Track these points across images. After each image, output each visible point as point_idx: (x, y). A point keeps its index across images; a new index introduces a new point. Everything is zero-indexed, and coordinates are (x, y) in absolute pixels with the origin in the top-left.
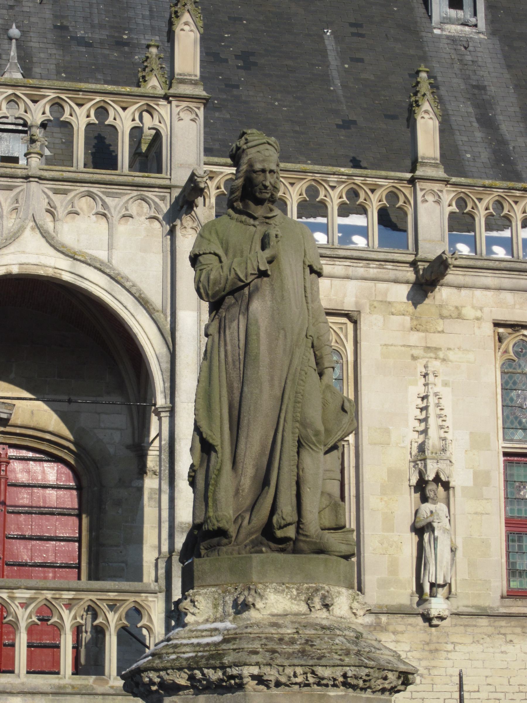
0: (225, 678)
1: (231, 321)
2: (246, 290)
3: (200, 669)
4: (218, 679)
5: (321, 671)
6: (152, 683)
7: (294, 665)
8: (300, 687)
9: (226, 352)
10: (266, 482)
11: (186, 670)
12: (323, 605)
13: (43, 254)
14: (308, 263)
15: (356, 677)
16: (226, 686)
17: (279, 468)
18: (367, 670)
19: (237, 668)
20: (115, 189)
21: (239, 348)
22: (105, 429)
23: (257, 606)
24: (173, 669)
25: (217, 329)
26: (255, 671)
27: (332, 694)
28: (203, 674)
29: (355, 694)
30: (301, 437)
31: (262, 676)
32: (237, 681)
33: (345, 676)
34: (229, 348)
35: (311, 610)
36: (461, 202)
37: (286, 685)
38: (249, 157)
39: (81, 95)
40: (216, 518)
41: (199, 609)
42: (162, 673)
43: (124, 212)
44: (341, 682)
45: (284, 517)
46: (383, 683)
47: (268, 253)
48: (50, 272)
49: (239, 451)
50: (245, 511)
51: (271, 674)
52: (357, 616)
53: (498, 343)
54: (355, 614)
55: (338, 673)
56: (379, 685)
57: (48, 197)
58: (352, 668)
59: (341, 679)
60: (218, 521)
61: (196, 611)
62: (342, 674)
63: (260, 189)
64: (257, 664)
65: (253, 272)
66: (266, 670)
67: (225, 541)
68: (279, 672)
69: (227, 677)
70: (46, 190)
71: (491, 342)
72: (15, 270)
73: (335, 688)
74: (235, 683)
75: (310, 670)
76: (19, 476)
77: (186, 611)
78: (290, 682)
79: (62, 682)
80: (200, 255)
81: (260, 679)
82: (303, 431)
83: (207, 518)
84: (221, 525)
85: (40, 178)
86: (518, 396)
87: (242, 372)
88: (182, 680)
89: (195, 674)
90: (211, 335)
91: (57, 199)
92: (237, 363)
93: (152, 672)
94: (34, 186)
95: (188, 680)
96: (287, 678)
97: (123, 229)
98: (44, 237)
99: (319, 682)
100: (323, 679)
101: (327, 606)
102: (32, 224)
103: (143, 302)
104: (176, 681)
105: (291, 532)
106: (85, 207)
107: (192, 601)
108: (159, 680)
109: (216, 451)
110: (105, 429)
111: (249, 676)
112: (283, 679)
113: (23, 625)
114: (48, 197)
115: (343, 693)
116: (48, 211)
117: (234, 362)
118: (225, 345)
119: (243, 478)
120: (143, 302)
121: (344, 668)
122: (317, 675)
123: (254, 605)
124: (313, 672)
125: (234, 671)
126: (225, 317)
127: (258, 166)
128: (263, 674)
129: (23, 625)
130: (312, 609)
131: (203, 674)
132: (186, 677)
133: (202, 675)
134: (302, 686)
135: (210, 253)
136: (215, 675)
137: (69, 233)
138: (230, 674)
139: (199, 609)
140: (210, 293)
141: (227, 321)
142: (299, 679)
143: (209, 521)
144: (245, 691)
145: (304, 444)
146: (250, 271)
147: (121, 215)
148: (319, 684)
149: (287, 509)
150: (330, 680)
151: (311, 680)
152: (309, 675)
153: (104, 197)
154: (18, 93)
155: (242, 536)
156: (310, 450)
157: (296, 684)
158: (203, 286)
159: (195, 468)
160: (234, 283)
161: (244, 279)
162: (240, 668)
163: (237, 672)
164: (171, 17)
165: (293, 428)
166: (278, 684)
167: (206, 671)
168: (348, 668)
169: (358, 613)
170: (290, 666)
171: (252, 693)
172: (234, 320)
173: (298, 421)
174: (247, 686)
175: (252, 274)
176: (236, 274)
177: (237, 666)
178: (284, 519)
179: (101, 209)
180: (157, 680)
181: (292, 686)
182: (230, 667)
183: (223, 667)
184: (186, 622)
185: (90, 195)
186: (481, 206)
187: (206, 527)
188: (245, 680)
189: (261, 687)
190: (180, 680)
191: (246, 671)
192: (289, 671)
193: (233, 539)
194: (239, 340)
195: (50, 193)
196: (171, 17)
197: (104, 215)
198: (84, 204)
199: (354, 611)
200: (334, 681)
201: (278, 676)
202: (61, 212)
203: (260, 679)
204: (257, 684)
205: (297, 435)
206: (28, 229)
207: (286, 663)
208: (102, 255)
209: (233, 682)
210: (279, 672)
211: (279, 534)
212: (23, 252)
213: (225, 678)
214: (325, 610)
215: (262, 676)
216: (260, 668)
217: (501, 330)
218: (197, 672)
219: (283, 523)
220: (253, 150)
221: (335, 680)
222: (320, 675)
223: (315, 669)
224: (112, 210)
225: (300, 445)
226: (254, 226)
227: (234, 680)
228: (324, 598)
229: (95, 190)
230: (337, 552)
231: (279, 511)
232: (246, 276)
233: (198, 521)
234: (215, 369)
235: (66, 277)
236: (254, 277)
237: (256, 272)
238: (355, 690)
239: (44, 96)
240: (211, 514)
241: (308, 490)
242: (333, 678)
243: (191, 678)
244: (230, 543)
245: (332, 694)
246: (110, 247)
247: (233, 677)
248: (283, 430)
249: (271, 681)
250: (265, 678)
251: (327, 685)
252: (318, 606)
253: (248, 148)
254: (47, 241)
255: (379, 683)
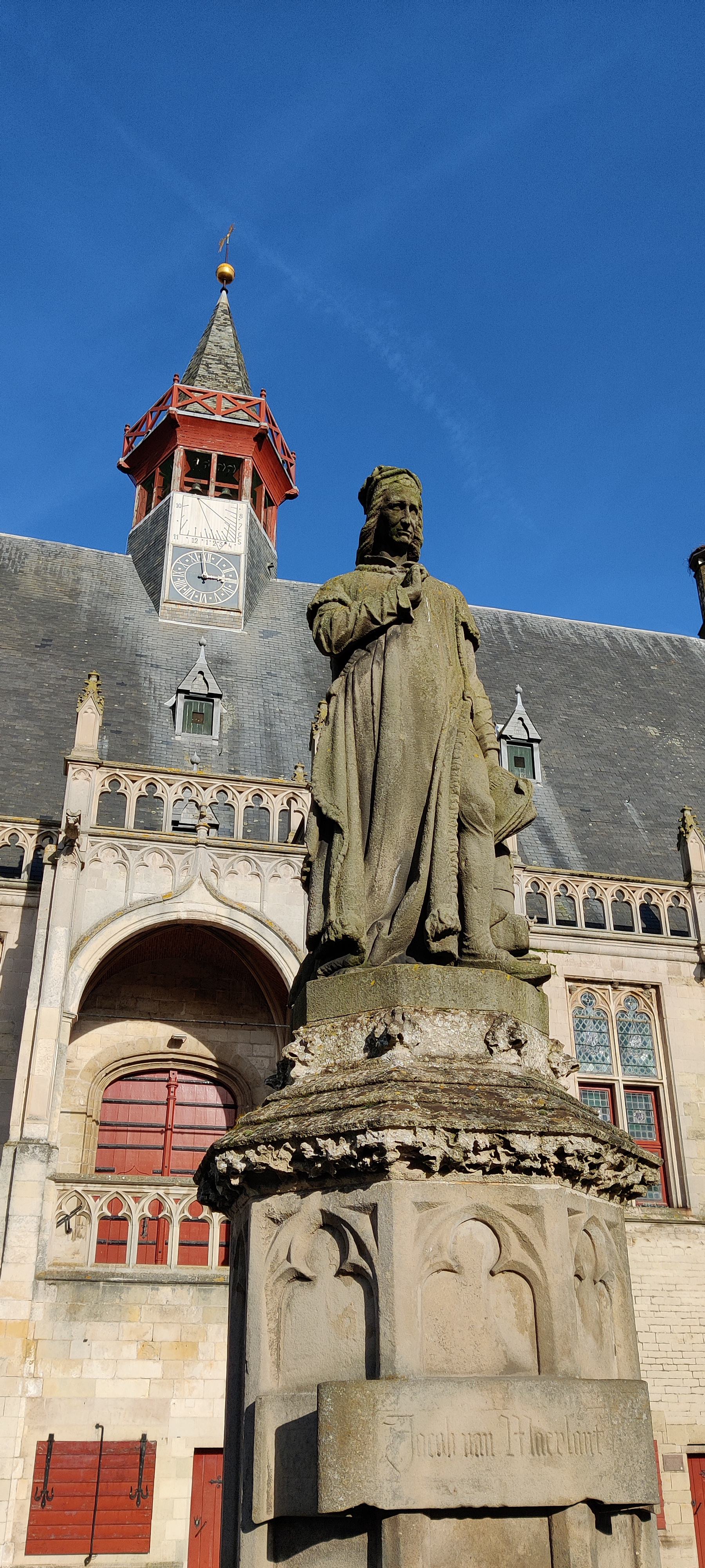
0: (355, 1153)
1: (362, 675)
2: (382, 638)
3: (312, 1140)
4: (343, 1157)
5: (520, 1143)
6: (232, 1171)
7: (474, 1131)
8: (484, 1173)
9: (354, 711)
10: (413, 875)
11: (288, 1145)
12: (511, 1043)
13: (207, 904)
14: (461, 620)
15: (581, 1157)
16: (356, 1169)
17: (432, 854)
18: (597, 1146)
19: (375, 1134)
20: (266, 855)
21: (373, 704)
22: (257, 1056)
23: (407, 1039)
24: (266, 1144)
25: (343, 687)
26: (408, 1138)
27: (537, 1187)
28: (317, 1149)
29: (574, 1192)
30: (463, 816)
31: (420, 1148)
32: (375, 1158)
33: (561, 1153)
34: (359, 706)
35: (491, 1052)
36: (535, 884)
37: (462, 1170)
38: (384, 488)
39: (241, 784)
40: (341, 923)
41: (313, 1055)
42: (251, 1154)
43: (273, 873)
44: (555, 1165)
45: (443, 918)
46: (615, 1176)
47: (410, 590)
48: (212, 918)
49: (373, 834)
50: (385, 918)
51: (435, 1145)
52: (559, 1075)
53: (569, 994)
54: (555, 1071)
55: (550, 1145)
56: (609, 1179)
57: (213, 860)
58: (574, 1139)
59: (555, 1159)
60: (343, 926)
61: (308, 1057)
62: (555, 1148)
63: (398, 530)
64: (411, 1127)
65: (391, 611)
66: (425, 1136)
67: (354, 958)
68: (448, 1141)
69: (357, 1150)
70: (212, 855)
71: (565, 993)
72: (184, 916)
73: (543, 1177)
74: (372, 1162)
75: (502, 1140)
76: (185, 1097)
77: (293, 1058)
78: (468, 1162)
79: (209, 1273)
80: (321, 604)
81: (415, 1157)
82: (465, 806)
83: (327, 926)
84: (348, 932)
85: (206, 844)
86: (588, 1036)
87: (377, 734)
88: (281, 1161)
89: (304, 1150)
90: (334, 695)
91: (221, 862)
92: (371, 723)
93: (232, 1151)
94: (202, 850)
95: (290, 1163)
96: (462, 1154)
97: (273, 886)
98: (208, 890)
99: (517, 1163)
100: (524, 1157)
101: (517, 1045)
102: (199, 880)
103: (288, 943)
104: (272, 1165)
105: (451, 944)
106: (242, 868)
107: (303, 1043)
108: (244, 1165)
109: (341, 831)
110: (257, 1056)
111: (397, 1147)
112: (457, 1156)
113: (176, 1219)
114: (213, 860)
115: (558, 1187)
116: (212, 871)
117: (365, 722)
118: (354, 703)
119: (379, 871)
120: (288, 943)
121: (559, 1138)
122: (513, 1150)
123: (400, 1037)
124: (507, 1144)
125: (369, 1139)
126: (353, 673)
127: (395, 499)
128: (421, 1145)
129: (176, 1219)
130: (493, 1048)
131: (317, 1149)
132: (289, 1157)
133: (315, 1152)
134: (488, 1169)
135: (334, 600)
136: (338, 1150)
137: (229, 888)
138: (363, 1145)
139: (313, 1055)
140: (334, 640)
141: (356, 676)
142: (484, 1157)
143: (330, 928)
144: (389, 1179)
145: (467, 825)
146: (387, 609)
147: (271, 875)
148: (515, 1168)
149: (446, 911)
150: (535, 1159)
151: (505, 1160)
152: (500, 1149)
153: (258, 861)
154: (191, 781)
155: (379, 952)
156: (475, 832)
157: (477, 1166)
158: (325, 632)
159: (310, 859)
160: (365, 627)
161: (379, 619)
162: (380, 1132)
163: (376, 1140)
164: (312, 730)
165: (451, 802)
166: (448, 1165)
167: (321, 1142)
168: (566, 1139)
169: (559, 1069)
170: (467, 1131)
171: (401, 1182)
172: (366, 672)
173: (456, 793)
174: (392, 1169)
175: (390, 614)
176: (369, 612)
177: (376, 1129)
178: (441, 922)
179: (255, 871)
180: (241, 1166)
181: (471, 1170)
182: (363, 1132)
183: (350, 1136)
184: (293, 1076)
185: (247, 859)
186: (551, 888)
187: (326, 937)
188: (391, 1156)
189: (418, 1172)
190: (278, 1161)
191: (390, 1139)
192: (466, 1140)
193: (368, 953)
194: (372, 694)
195: (215, 857)
196: (312, 730)
197: (258, 875)
198: (241, 866)
199: (554, 1066)
200: (542, 1163)
201: (446, 1149)
202: (223, 871)
203: (415, 1157)
204: (410, 1167)
205: (457, 811)
206: (196, 883)
207: (460, 1124)
208: (256, 906)
209: (367, 1160)
210: (448, 1141)
211: (435, 947)
212: (191, 902)
213: (355, 1153)
214: (513, 1051)
215: (420, 1148)
216: (415, 1134)
217: (571, 984)
218: (305, 1145)
219: (441, 927)
220: (388, 480)
221: (544, 1159)
222: (518, 1149)
223: (509, 1137)
224: (264, 871)
225: (461, 829)
226: (391, 573)
227: (370, 1156)
228: (511, 1033)
229: (251, 854)
230: (524, 973)
231: (434, 912)
232: (382, 616)
233: (313, 931)
234: (340, 738)
235: (225, 922)
236: (391, 619)
237: (395, 611)
238: (574, 1182)
239: (213, 784)
240: (333, 916)
241: (475, 890)
242: (540, 1155)
243: (298, 1157)
244: (362, 962)
245: (537, 1187)
246: (262, 900)
247: (367, 1151)
248: (437, 804)
249: (434, 1158)
250: (425, 1152)
251: (529, 1171)
252: (503, 1044)
253: (383, 478)
254: (211, 893)
255: (610, 1176)
